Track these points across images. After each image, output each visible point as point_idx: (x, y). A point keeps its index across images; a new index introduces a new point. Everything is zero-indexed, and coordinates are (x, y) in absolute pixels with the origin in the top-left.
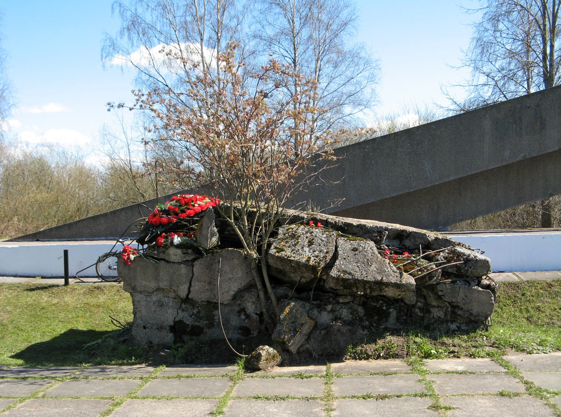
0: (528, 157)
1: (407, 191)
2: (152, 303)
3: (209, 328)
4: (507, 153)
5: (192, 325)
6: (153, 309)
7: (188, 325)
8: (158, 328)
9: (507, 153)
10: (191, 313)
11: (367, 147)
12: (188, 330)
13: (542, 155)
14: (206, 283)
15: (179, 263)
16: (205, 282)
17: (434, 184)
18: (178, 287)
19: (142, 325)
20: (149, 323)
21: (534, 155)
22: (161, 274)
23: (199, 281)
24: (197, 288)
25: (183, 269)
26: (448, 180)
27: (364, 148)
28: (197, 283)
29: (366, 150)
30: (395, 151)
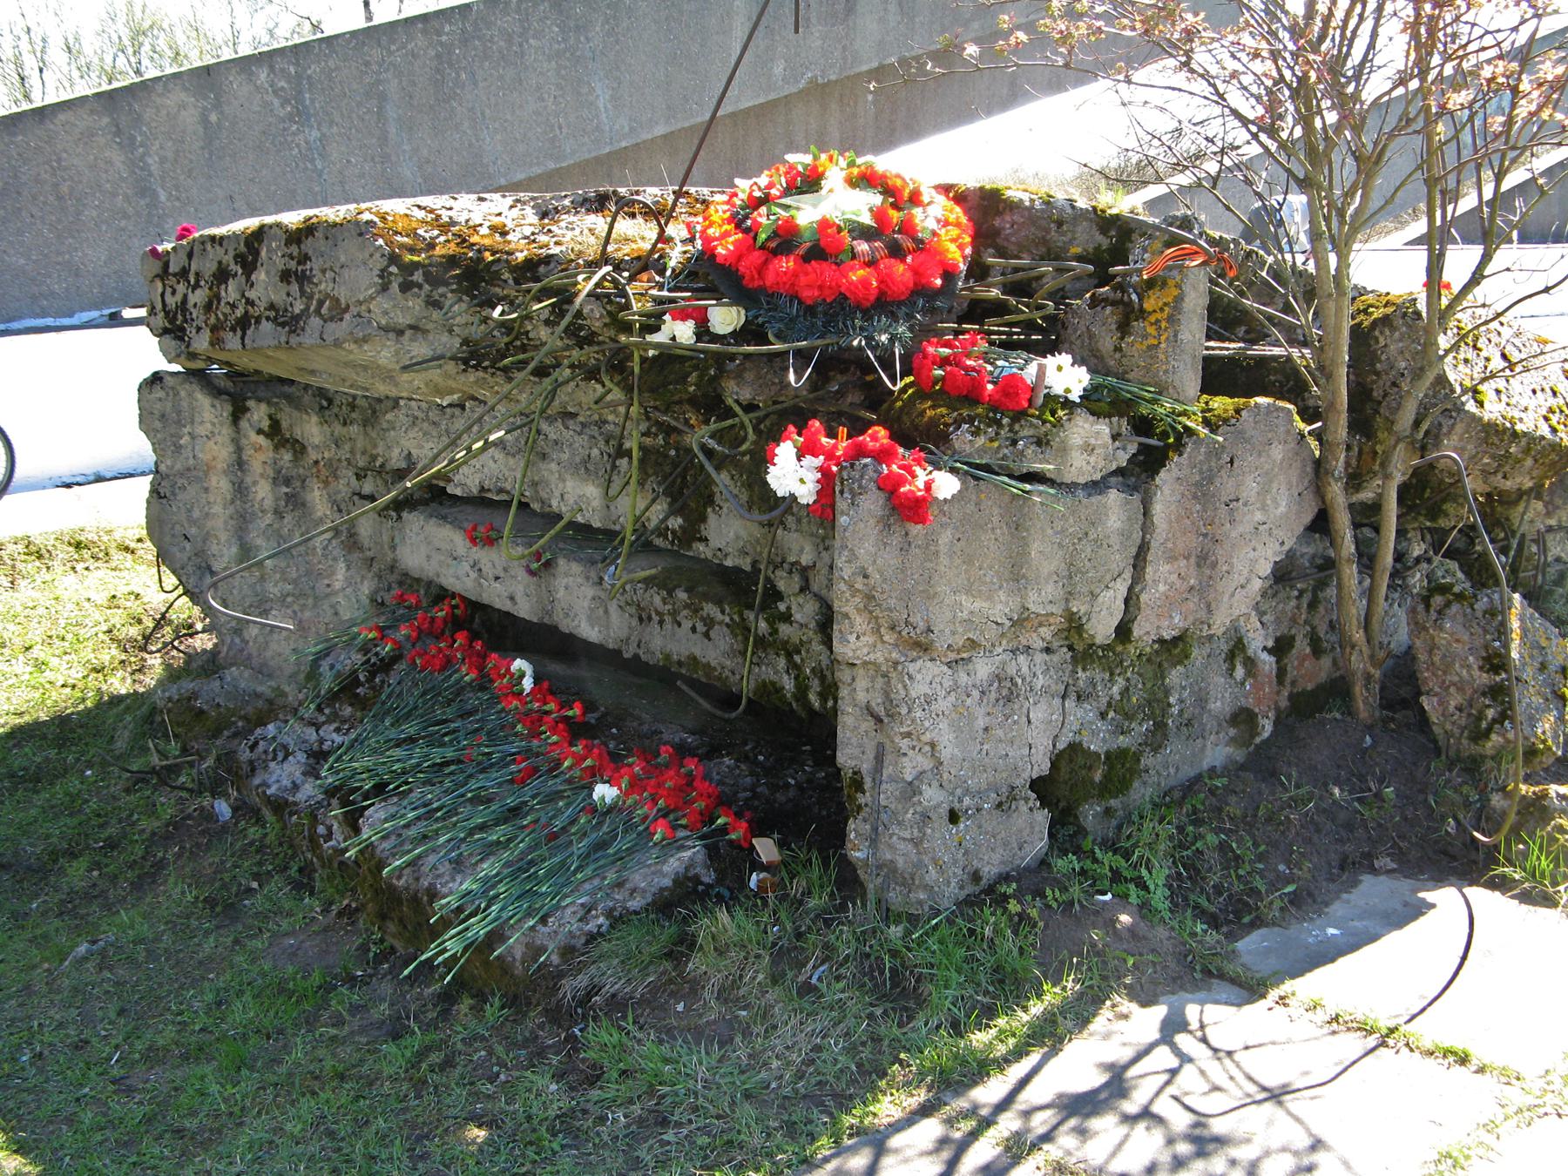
0: (820, 81)
1: (551, 165)
2: (976, 694)
3: (1156, 749)
4: (779, 69)
5: (1108, 754)
6: (981, 723)
7: (1097, 755)
8: (1000, 805)
9: (779, 69)
10: (1104, 701)
11: (447, 29)
12: (1098, 776)
13: (847, 77)
14: (1193, 560)
15: (1096, 487)
16: (1187, 558)
17: (617, 146)
18: (1094, 596)
19: (944, 811)
20: (967, 791)
21: (833, 77)
22: (1035, 548)
23: (1172, 558)
24: (1162, 588)
25: (1115, 507)
26: (650, 137)
27: (439, 33)
28: (1165, 568)
29: (444, 38)
30: (521, 45)
